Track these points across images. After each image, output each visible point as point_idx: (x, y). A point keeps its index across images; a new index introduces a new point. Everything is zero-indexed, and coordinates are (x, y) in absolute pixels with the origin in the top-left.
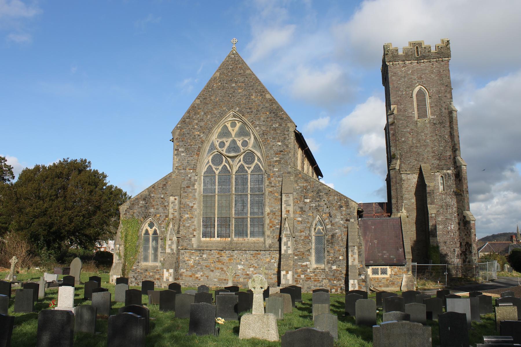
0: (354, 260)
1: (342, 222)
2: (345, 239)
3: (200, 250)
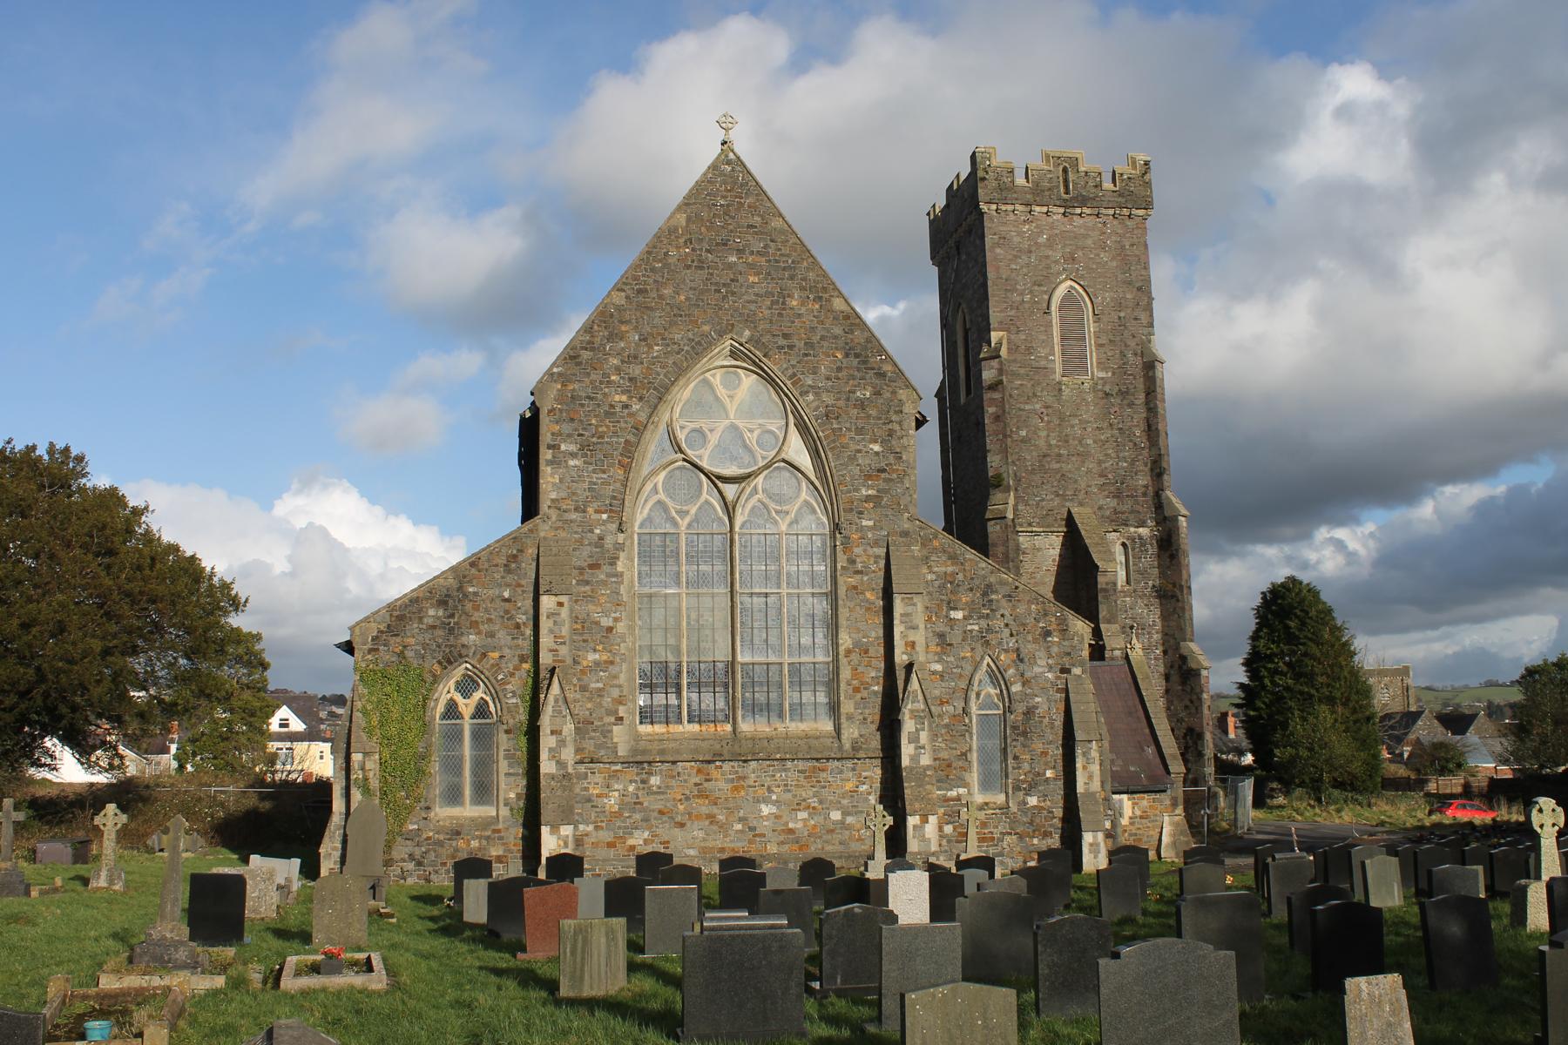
0: (1089, 777)
1: (1050, 675)
2: (1059, 723)
3: (641, 762)
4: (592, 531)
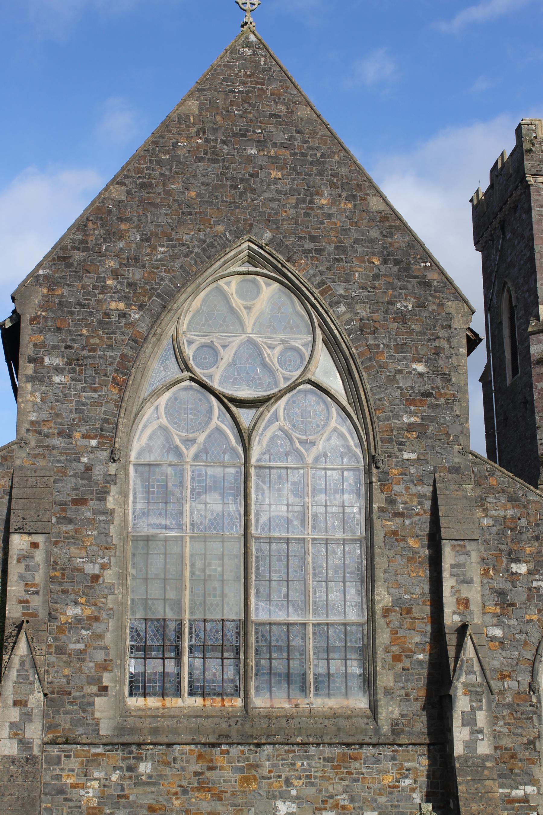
3: (128, 743)
4: (78, 460)
